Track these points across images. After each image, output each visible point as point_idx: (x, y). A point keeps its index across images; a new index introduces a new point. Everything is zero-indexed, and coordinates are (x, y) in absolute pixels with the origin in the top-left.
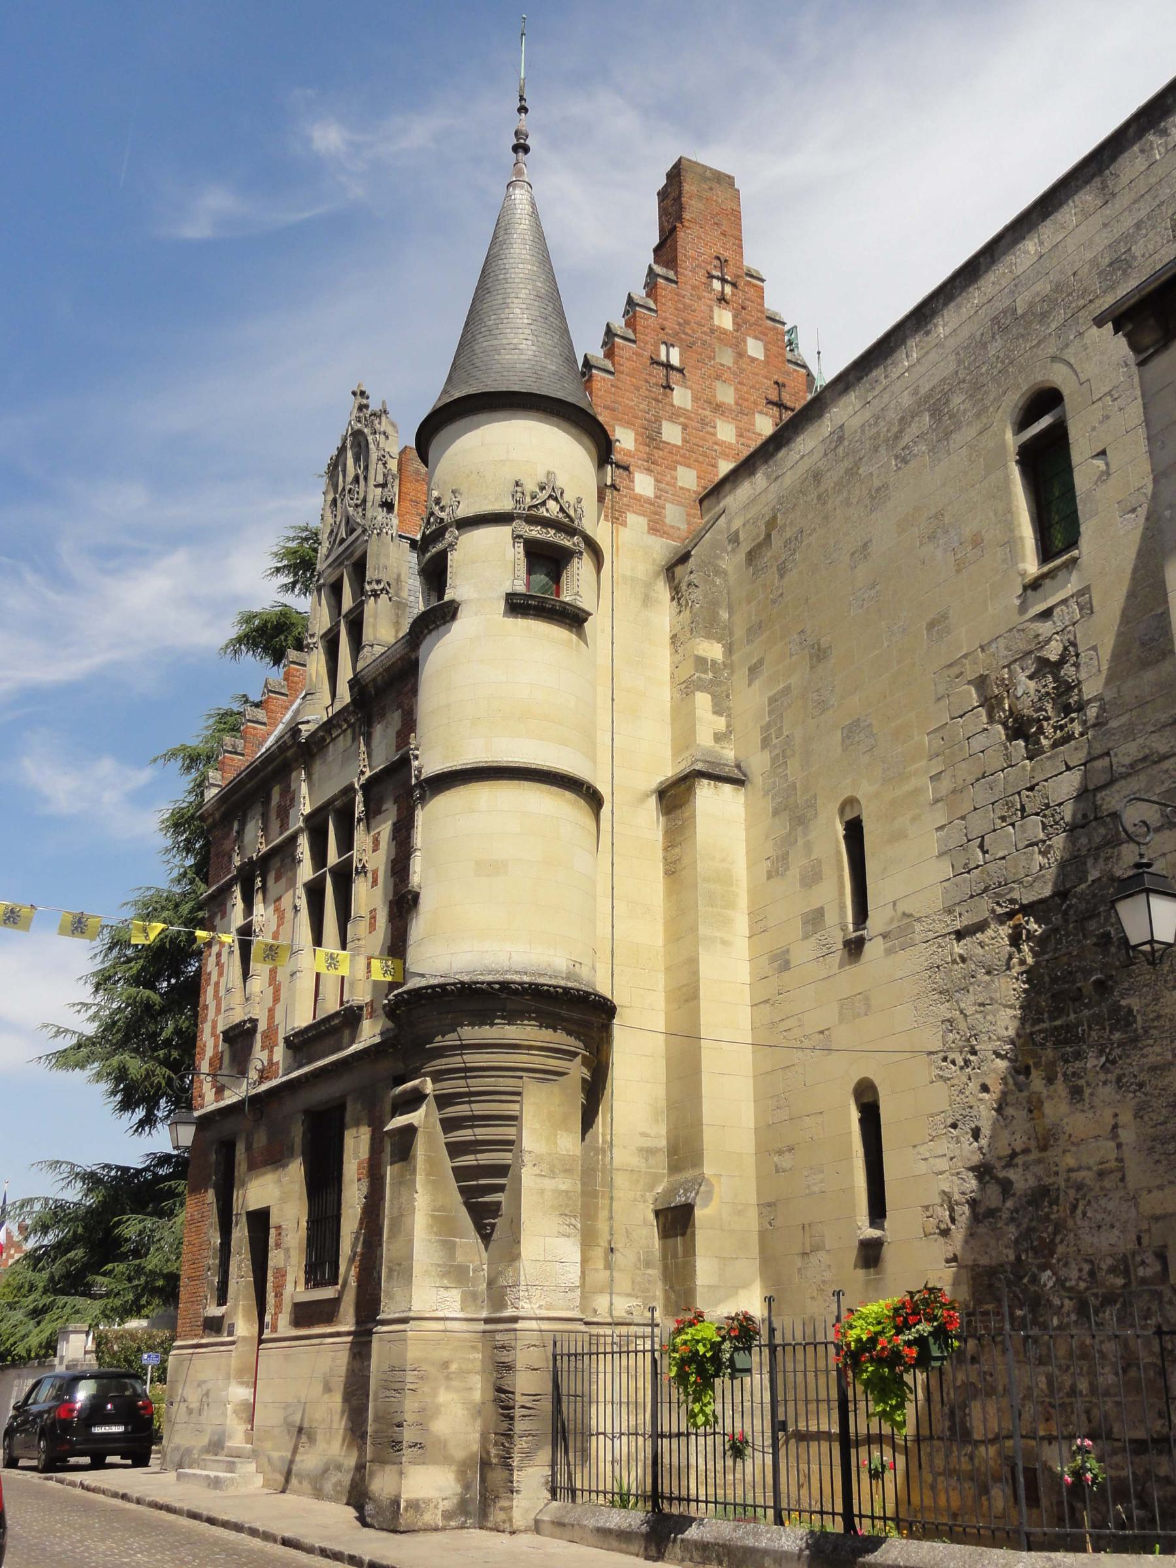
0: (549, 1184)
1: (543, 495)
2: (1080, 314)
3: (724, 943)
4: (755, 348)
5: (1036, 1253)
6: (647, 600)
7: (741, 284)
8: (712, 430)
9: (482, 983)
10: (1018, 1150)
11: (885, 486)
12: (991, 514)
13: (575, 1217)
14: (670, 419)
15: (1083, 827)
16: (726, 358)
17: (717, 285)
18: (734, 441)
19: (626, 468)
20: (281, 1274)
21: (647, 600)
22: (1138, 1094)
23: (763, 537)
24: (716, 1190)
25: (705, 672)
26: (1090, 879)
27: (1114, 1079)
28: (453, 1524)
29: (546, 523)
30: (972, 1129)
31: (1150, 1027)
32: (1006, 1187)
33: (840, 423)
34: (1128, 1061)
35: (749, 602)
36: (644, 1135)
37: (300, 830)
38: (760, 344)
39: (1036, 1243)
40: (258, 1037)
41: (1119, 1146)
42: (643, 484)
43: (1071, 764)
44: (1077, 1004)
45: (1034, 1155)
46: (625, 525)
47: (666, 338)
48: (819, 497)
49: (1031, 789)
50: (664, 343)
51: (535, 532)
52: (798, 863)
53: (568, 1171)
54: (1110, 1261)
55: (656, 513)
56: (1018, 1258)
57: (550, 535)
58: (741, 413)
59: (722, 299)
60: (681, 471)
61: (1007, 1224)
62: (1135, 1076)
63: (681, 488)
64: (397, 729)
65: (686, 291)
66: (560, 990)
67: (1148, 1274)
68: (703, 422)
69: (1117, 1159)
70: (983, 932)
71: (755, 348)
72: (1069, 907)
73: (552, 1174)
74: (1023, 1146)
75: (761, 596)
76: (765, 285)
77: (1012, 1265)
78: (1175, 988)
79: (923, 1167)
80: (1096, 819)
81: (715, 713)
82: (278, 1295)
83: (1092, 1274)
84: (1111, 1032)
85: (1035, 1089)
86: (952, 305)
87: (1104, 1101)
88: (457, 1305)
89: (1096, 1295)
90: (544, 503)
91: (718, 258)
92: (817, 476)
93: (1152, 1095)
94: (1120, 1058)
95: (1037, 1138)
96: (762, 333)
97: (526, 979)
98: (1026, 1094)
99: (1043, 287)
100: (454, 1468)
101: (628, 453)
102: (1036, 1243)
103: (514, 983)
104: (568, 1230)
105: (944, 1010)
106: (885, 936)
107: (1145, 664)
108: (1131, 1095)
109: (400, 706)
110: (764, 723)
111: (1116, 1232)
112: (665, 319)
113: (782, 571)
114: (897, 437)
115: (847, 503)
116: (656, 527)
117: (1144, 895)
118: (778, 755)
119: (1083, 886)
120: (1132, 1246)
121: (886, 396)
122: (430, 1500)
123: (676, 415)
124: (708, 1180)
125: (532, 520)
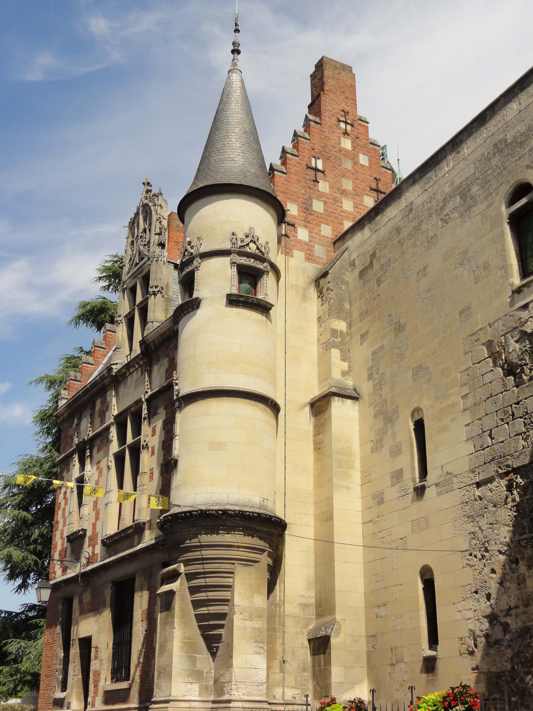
0: (248, 624)
1: (247, 240)
3: (347, 488)
4: (363, 160)
5: (523, 665)
6: (305, 298)
7: (356, 125)
8: (340, 204)
10: (512, 606)
11: (436, 236)
14: (317, 199)
16: (348, 165)
17: (343, 125)
18: (352, 211)
21: (305, 298)
23: (368, 263)
24: (343, 627)
25: (337, 337)
30: (486, 594)
32: (506, 627)
36: (302, 596)
37: (112, 424)
40: (87, 539)
42: (303, 234)
46: (293, 257)
48: (399, 242)
49: (518, 403)
50: (314, 157)
51: (243, 261)
53: (260, 617)
55: (309, 250)
56: (513, 668)
57: (251, 262)
58: (356, 195)
59: (346, 133)
60: (323, 226)
61: (506, 649)
63: (323, 236)
65: (326, 129)
66: (256, 515)
68: (336, 200)
70: (491, 483)
71: (363, 160)
75: (368, 296)
79: (459, 616)
81: (342, 360)
82: (96, 686)
85: (522, 572)
88: (197, 693)
90: (248, 245)
91: (343, 111)
92: (398, 230)
95: (523, 600)
98: (516, 574)
101: (294, 217)
102: (523, 659)
104: (260, 650)
106: (437, 485)
109: (168, 356)
113: (379, 282)
114: (442, 209)
116: (310, 258)
121: (436, 186)
123: (321, 196)
124: (338, 622)
125: (241, 254)
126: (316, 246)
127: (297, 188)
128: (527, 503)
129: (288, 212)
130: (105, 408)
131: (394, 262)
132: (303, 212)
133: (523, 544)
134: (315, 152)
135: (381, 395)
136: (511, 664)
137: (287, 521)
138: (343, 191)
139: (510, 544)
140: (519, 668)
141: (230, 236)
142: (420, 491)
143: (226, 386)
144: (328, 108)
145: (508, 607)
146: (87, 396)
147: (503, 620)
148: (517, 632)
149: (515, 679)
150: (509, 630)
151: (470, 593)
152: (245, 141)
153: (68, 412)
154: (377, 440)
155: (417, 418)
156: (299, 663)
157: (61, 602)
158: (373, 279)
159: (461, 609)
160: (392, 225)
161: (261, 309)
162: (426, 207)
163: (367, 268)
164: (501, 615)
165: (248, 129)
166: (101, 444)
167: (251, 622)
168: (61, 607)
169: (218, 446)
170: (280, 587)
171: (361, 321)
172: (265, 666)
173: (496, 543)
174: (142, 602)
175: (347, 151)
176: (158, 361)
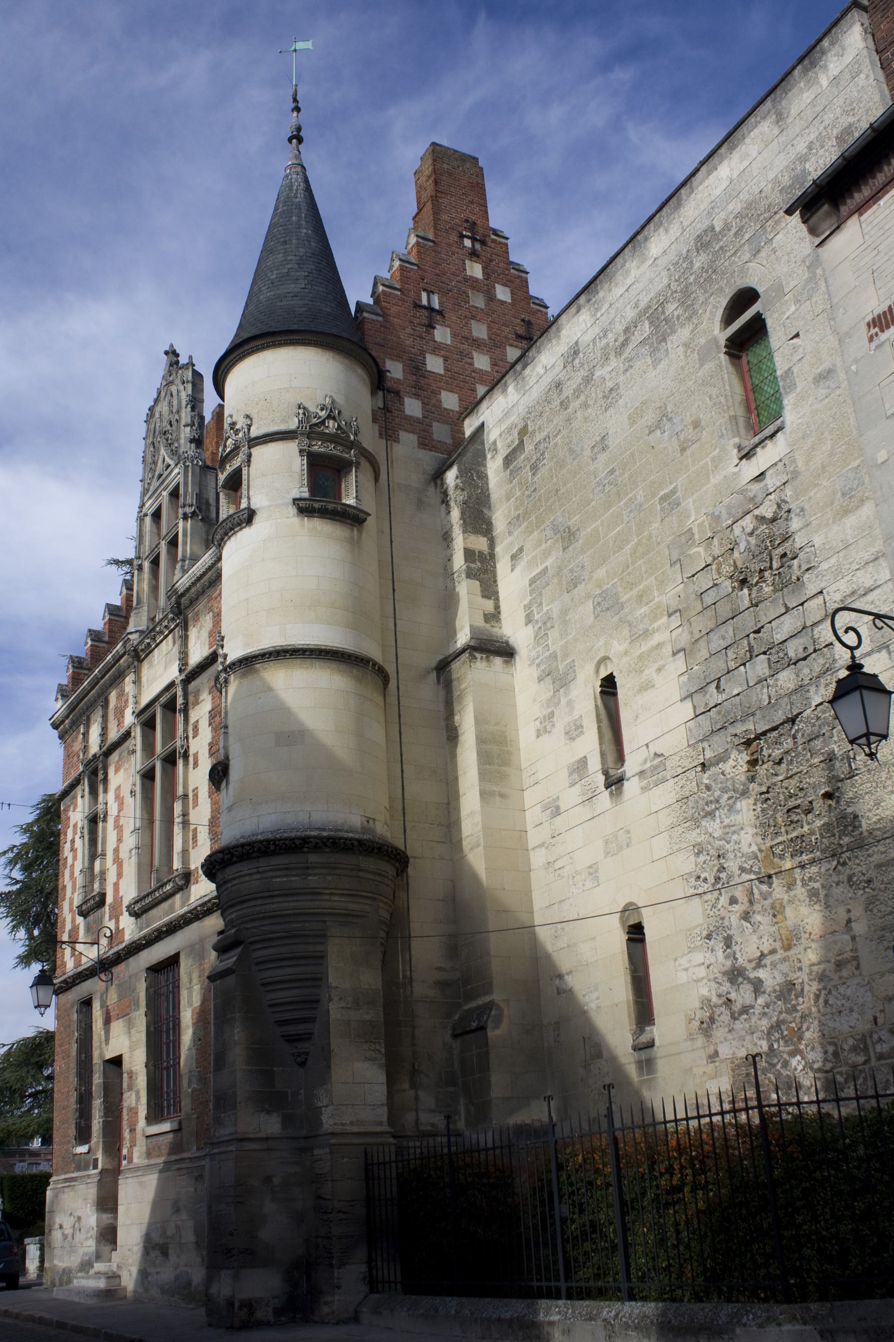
1: (323, 414)
2: (768, 224)
3: (502, 796)
4: (503, 293)
5: (786, 1042)
10: (766, 952)
12: (707, 399)
13: (379, 1043)
15: (804, 659)
16: (478, 301)
17: (468, 243)
18: (489, 369)
20: (134, 1112)
22: (867, 890)
23: (517, 442)
24: (506, 1012)
25: (474, 562)
26: (814, 704)
27: (845, 879)
30: (724, 938)
31: (873, 829)
32: (757, 986)
33: (575, 339)
34: (857, 861)
35: (508, 499)
36: (439, 969)
38: (508, 290)
39: (786, 1033)
41: (853, 938)
42: (413, 407)
43: (791, 606)
44: (810, 816)
45: (781, 954)
46: (398, 442)
47: (425, 286)
48: (562, 403)
49: (758, 631)
50: (424, 290)
51: (318, 447)
52: (562, 721)
54: (851, 1042)
56: (771, 1048)
59: (474, 254)
61: (760, 1019)
62: (864, 874)
64: (208, 629)
67: (884, 1050)
69: (852, 950)
70: (724, 762)
71: (503, 293)
72: (797, 731)
74: (770, 948)
75: (518, 494)
76: (509, 242)
77: (767, 1054)
78: (892, 792)
79: (683, 977)
80: (815, 651)
81: (483, 597)
82: (132, 1130)
83: (836, 1054)
84: (840, 838)
85: (778, 896)
86: (661, 230)
87: (837, 900)
89: (841, 1073)
90: (323, 422)
91: (467, 221)
92: (558, 385)
93: (880, 889)
94: (850, 859)
95: (781, 939)
97: (325, 834)
98: (770, 901)
99: (735, 206)
101: (397, 381)
102: (786, 1033)
106: (641, 773)
107: (846, 512)
108: (861, 892)
109: (211, 610)
110: (526, 602)
111: (855, 1015)
112: (425, 271)
113: (534, 468)
114: (624, 344)
115: (585, 405)
117: (857, 694)
118: (540, 628)
119: (809, 711)
120: (868, 1026)
121: (612, 312)
123: (437, 349)
124: (498, 1005)
126: (435, 424)
128: (782, 787)
129: (388, 374)
130: (123, 704)
131: (556, 436)
133: (778, 851)
135: (547, 645)
136: (768, 1041)
137: (409, 853)
138: (474, 340)
139: (759, 854)
140: (782, 1047)
142: (614, 783)
143: (298, 642)
145: (759, 954)
147: (752, 976)
148: (775, 991)
149: (774, 1065)
150: (762, 990)
151: (699, 938)
154: (544, 717)
155: (603, 674)
157: (75, 1009)
158: (525, 466)
159: (687, 965)
160: (549, 380)
161: (349, 521)
162: (598, 344)
163: (514, 451)
164: (749, 966)
166: (119, 760)
168: (75, 1016)
172: (383, 1078)
173: (735, 856)
174: (192, 997)
175: (476, 280)
176: (197, 619)
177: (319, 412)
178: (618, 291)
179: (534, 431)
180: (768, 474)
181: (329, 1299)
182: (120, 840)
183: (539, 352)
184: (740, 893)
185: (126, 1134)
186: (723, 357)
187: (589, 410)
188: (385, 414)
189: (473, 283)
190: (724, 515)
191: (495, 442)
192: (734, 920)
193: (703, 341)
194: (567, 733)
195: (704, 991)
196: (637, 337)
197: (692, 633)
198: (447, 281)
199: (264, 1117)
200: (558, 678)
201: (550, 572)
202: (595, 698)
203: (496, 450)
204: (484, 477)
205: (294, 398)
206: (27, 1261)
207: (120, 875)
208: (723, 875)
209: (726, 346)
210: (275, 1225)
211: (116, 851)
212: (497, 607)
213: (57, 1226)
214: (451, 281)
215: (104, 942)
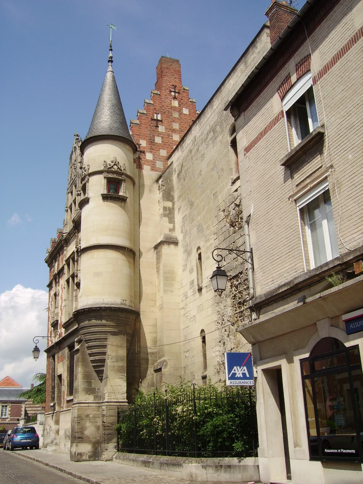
1: (112, 164)
3: (171, 291)
7: (181, 92)
8: (171, 137)
9: (94, 308)
13: (124, 373)
14: (158, 136)
16: (176, 115)
17: (173, 94)
19: (144, 152)
20: (64, 392)
28: (92, 459)
29: (113, 172)
37: (65, 264)
40: (59, 325)
42: (149, 156)
49: (234, 243)
50: (156, 113)
51: (110, 176)
53: (122, 360)
55: (153, 164)
57: (115, 176)
59: (175, 98)
63: (161, 156)
65: (163, 97)
66: (98, 308)
68: (169, 135)
71: (186, 111)
73: (117, 361)
75: (180, 187)
81: (169, 223)
82: (64, 399)
88: (93, 399)
96: (188, 106)
100: (92, 444)
101: (144, 148)
103: (113, 307)
104: (122, 377)
105: (218, 309)
113: (184, 179)
114: (206, 139)
115: (197, 159)
116: (153, 169)
122: (85, 453)
123: (159, 134)
125: (108, 172)
127: (145, 132)
131: (190, 169)
132: (149, 144)
134: (156, 110)
138: (173, 130)
141: (104, 163)
144: (165, 85)
146: (56, 250)
152: (112, 110)
153: (50, 259)
155: (199, 252)
156: (149, 383)
165: (115, 103)
167: (117, 363)
169: (97, 274)
170: (137, 345)
171: (178, 201)
175: (175, 107)
177: (111, 163)
178: (206, 119)
179: (185, 166)
180: (238, 189)
181: (104, 453)
182: (62, 303)
183: (187, 138)
184: (227, 328)
185: (62, 400)
186: (230, 147)
187: (198, 161)
188: (139, 160)
189: (174, 109)
190: (228, 202)
191: (175, 168)
192: (225, 337)
193: (225, 141)
194: (190, 271)
195: (218, 360)
196: (210, 137)
197: (219, 241)
198: (164, 109)
199: (88, 396)
200: (188, 253)
201: (187, 216)
202: (197, 260)
203: (175, 171)
204: (171, 180)
205: (102, 159)
206: (291, 460)
207: (62, 314)
208: (223, 322)
209: (231, 143)
210: (90, 430)
211: (61, 306)
212: (174, 226)
213: (46, 429)
214: (166, 109)
215: (58, 336)
